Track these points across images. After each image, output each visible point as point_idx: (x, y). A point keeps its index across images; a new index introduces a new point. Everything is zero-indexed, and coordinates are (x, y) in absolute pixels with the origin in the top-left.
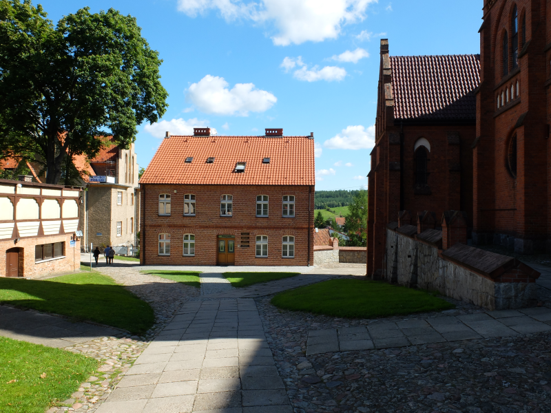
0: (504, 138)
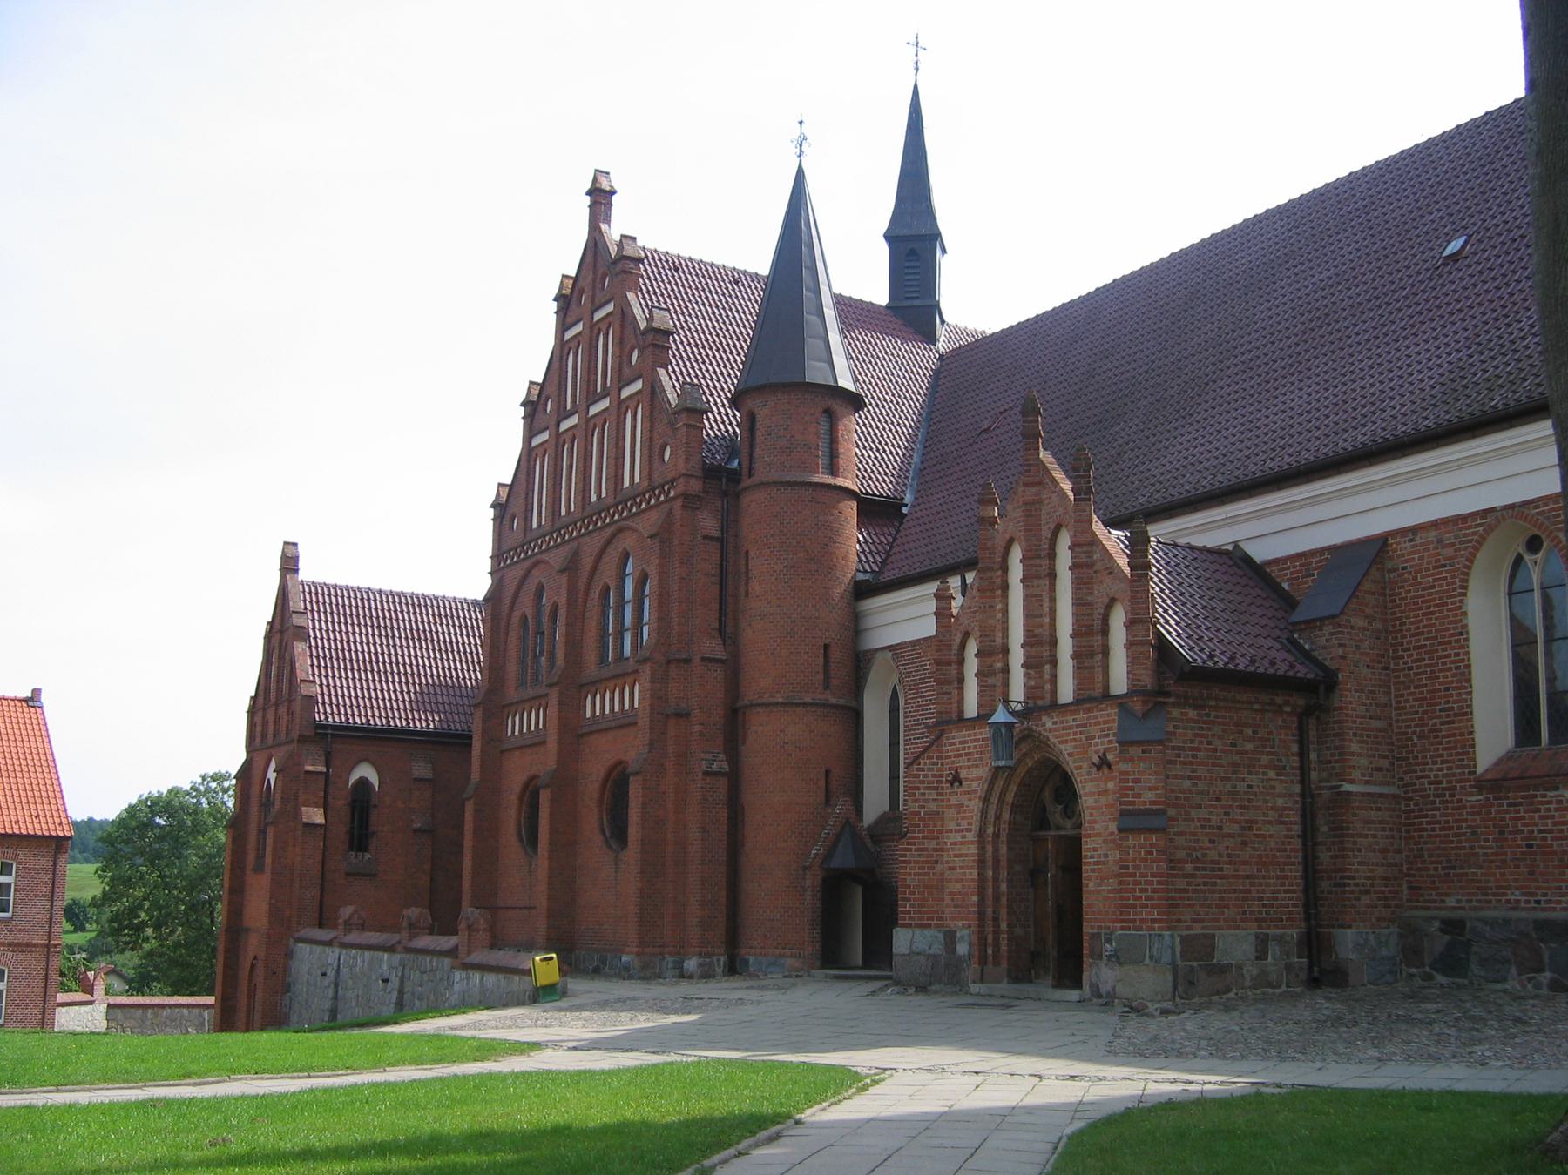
0: (517, 788)
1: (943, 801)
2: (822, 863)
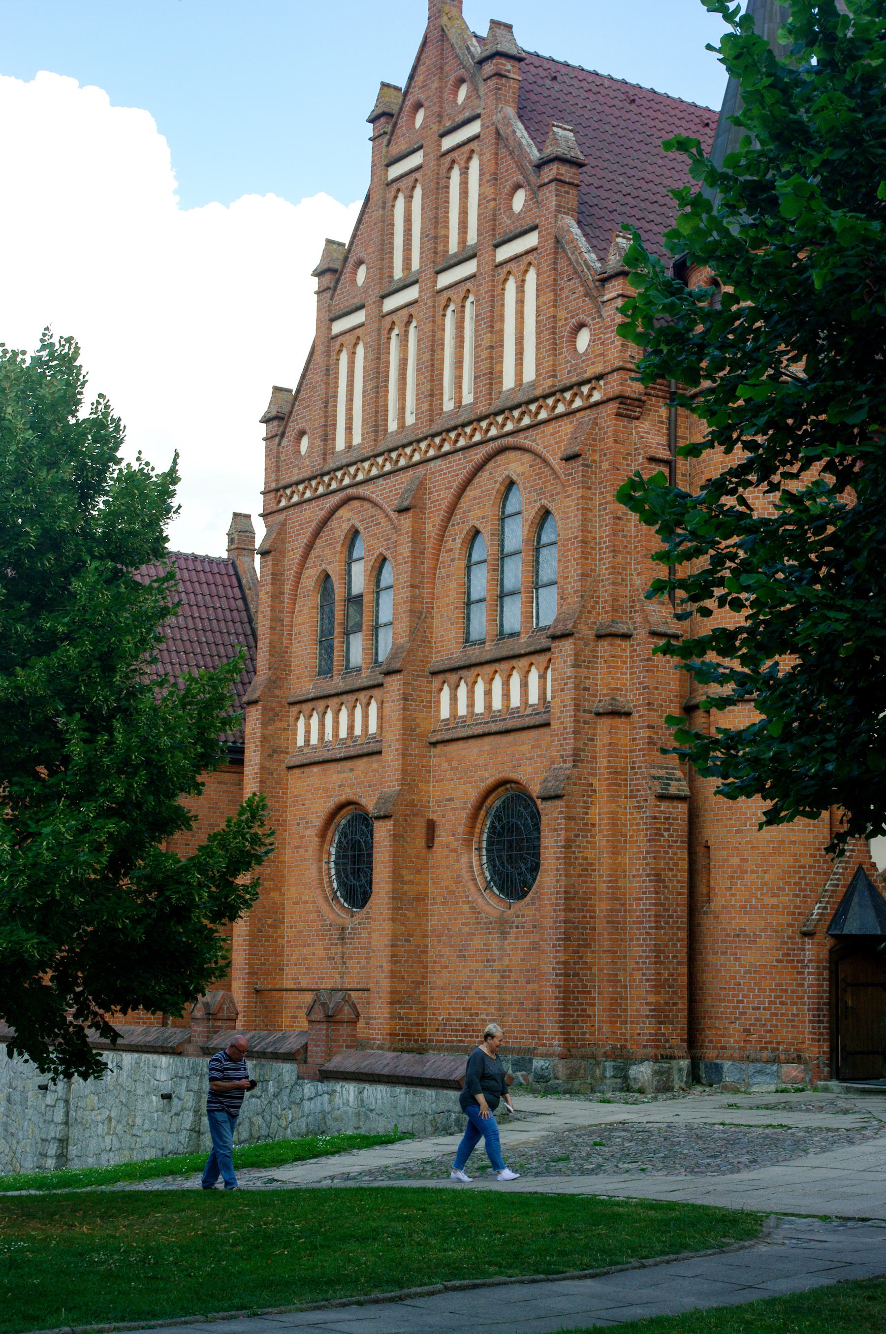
1: (586, 876)
2: (829, 928)
